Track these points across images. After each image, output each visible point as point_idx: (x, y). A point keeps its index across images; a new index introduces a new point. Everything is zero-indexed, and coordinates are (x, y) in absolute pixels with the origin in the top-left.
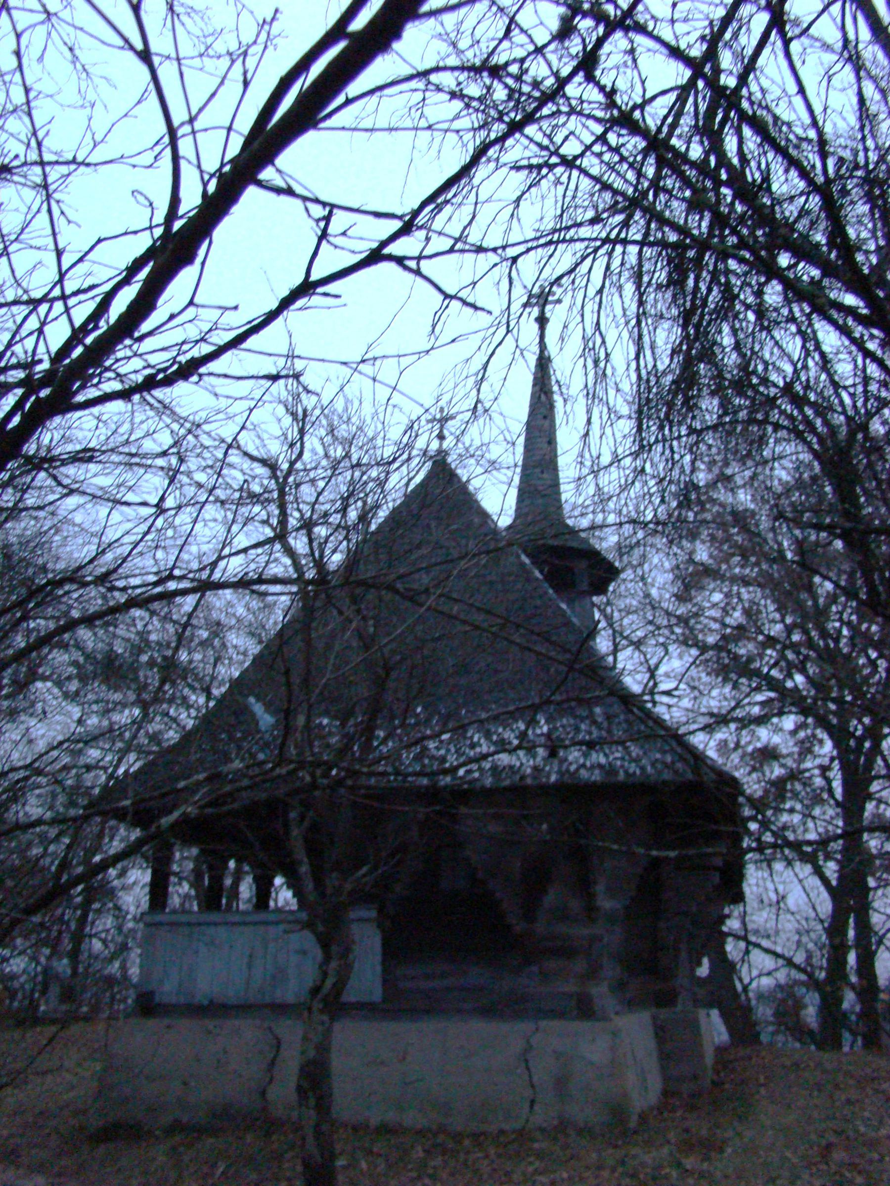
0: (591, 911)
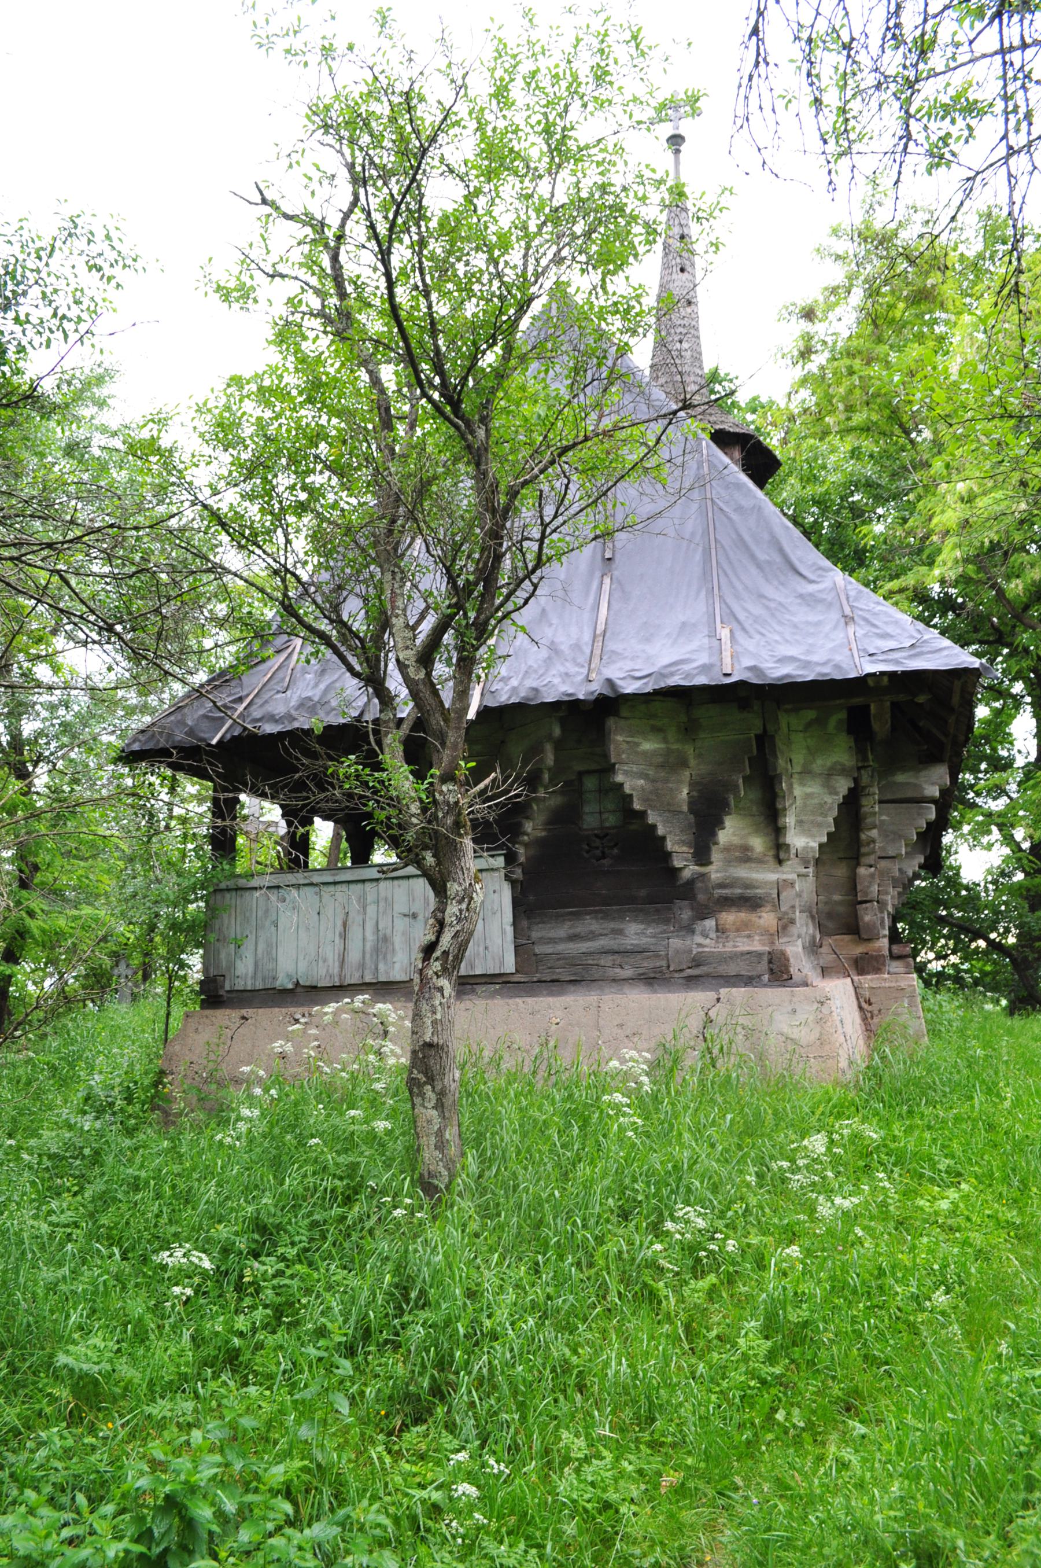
0: (779, 851)
